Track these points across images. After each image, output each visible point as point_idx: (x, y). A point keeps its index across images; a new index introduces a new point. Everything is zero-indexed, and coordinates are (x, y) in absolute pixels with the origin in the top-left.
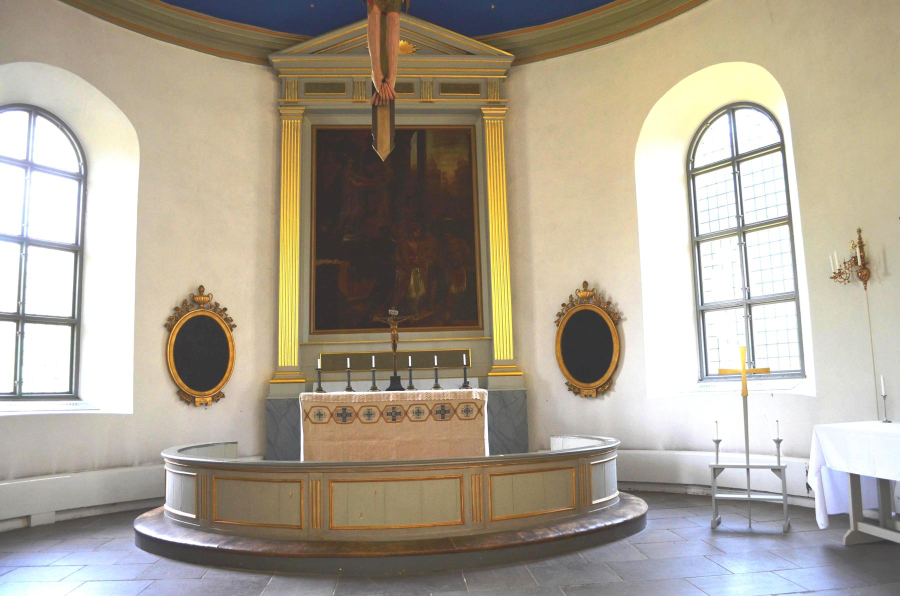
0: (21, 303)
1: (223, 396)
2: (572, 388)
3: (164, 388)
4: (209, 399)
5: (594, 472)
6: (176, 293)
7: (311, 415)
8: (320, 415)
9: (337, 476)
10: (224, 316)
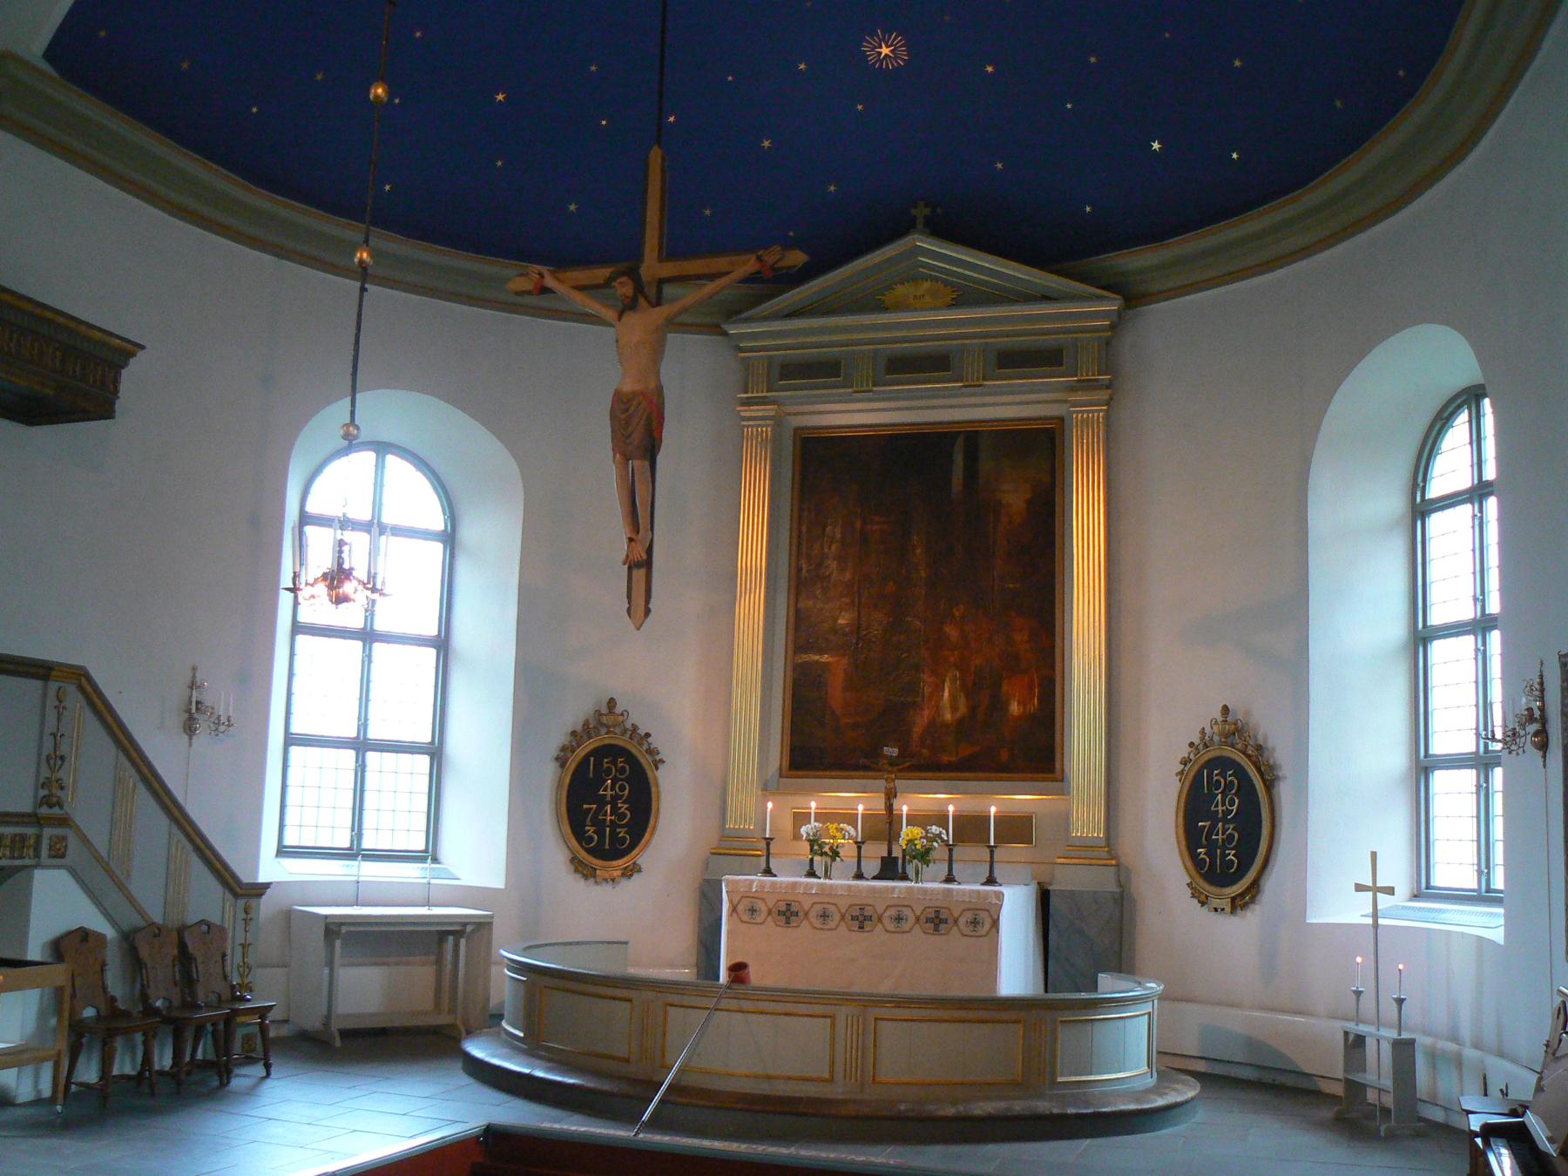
0: (363, 724)
1: (640, 870)
2: (1196, 894)
3: (555, 852)
4: (617, 873)
5: (1064, 1034)
6: (573, 712)
7: (740, 908)
8: (753, 911)
9: (675, 999)
10: (645, 747)
